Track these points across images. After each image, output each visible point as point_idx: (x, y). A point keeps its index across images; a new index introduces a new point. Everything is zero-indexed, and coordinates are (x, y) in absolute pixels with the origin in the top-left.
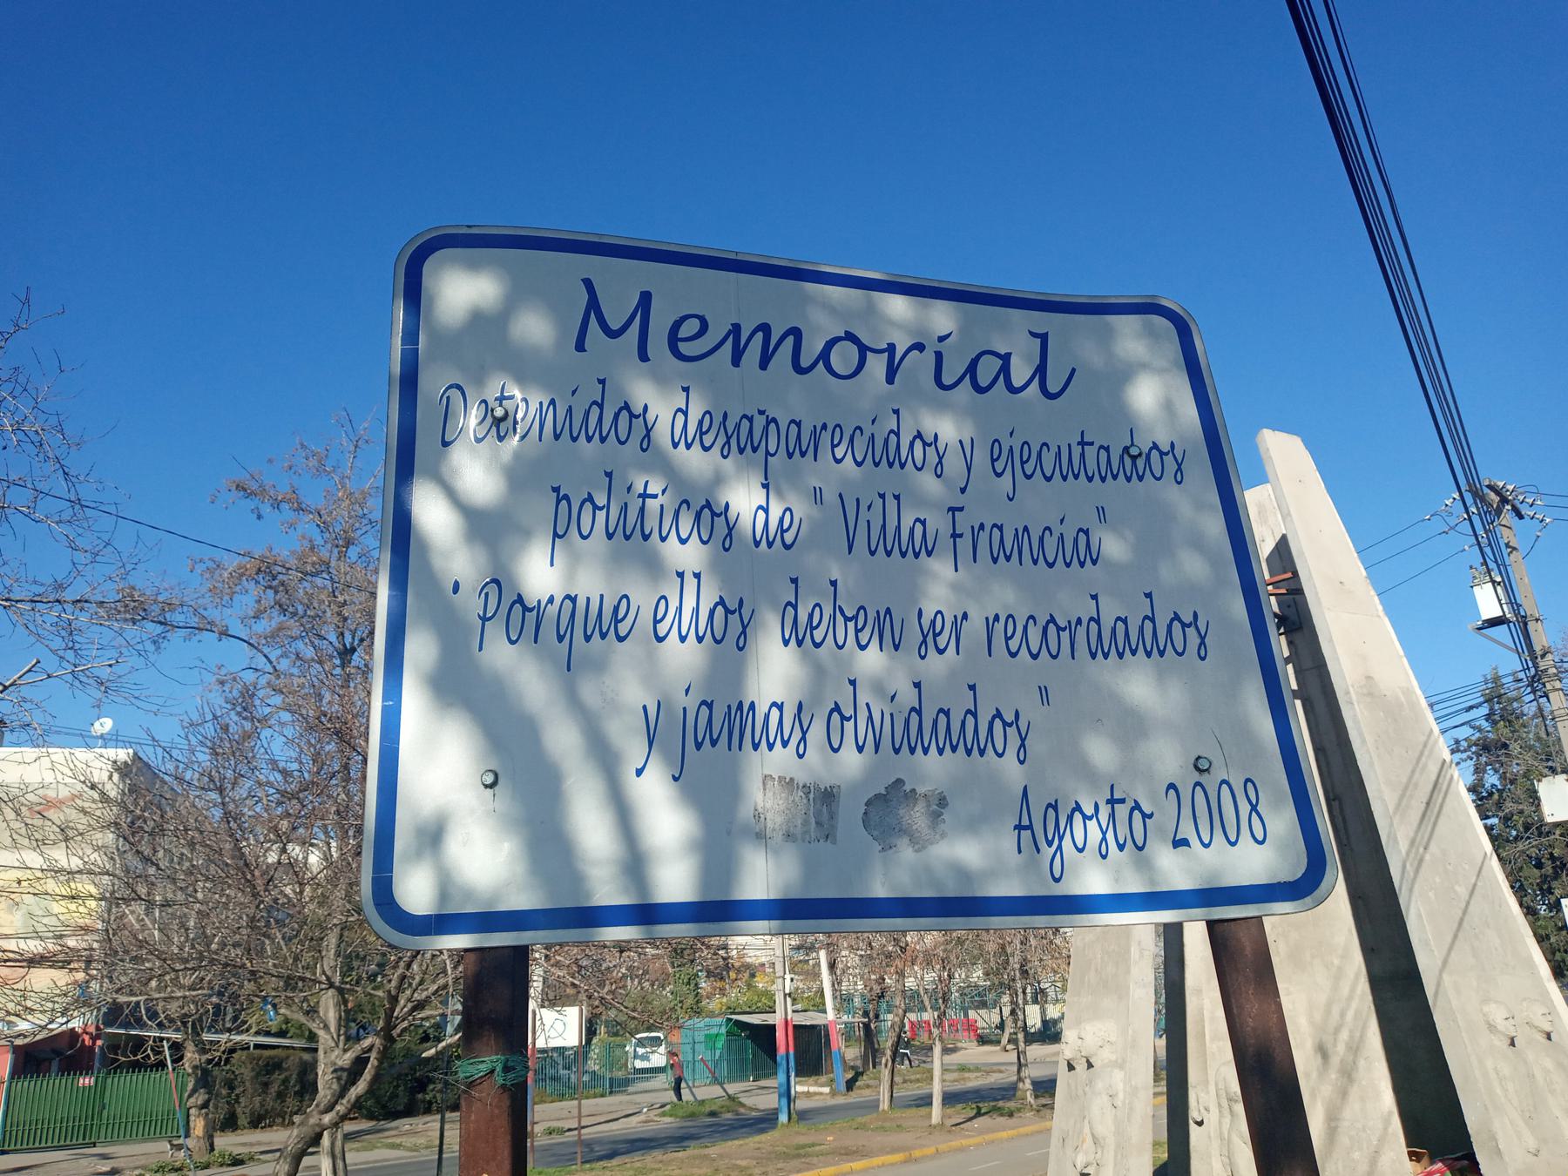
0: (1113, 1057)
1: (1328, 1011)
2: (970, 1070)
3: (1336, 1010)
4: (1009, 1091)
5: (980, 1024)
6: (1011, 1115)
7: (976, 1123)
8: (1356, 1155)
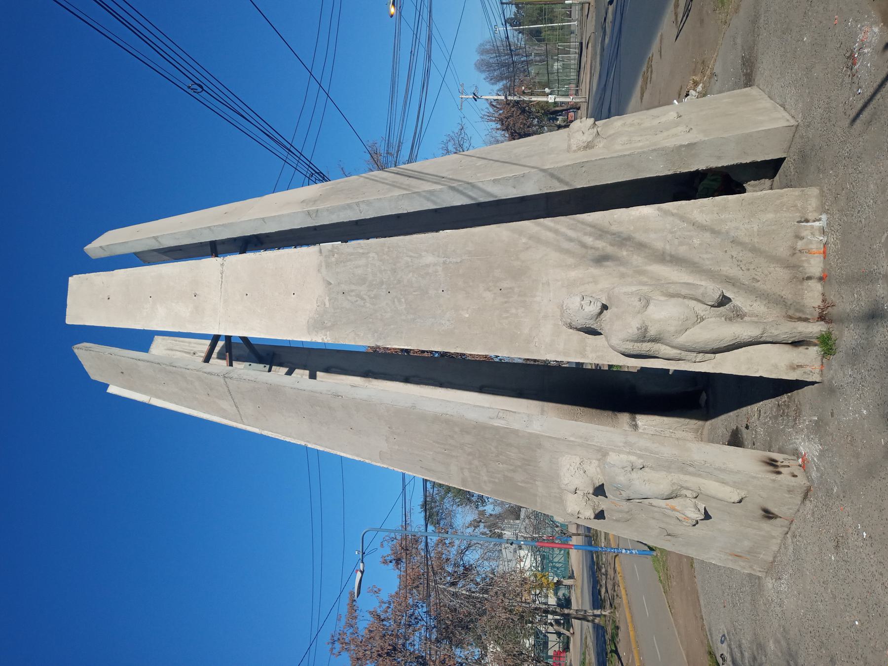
0: (595, 463)
1: (567, 252)
2: (584, 659)
3: (566, 245)
4: (599, 631)
5: (556, 648)
6: (617, 628)
7: (623, 654)
8: (697, 242)
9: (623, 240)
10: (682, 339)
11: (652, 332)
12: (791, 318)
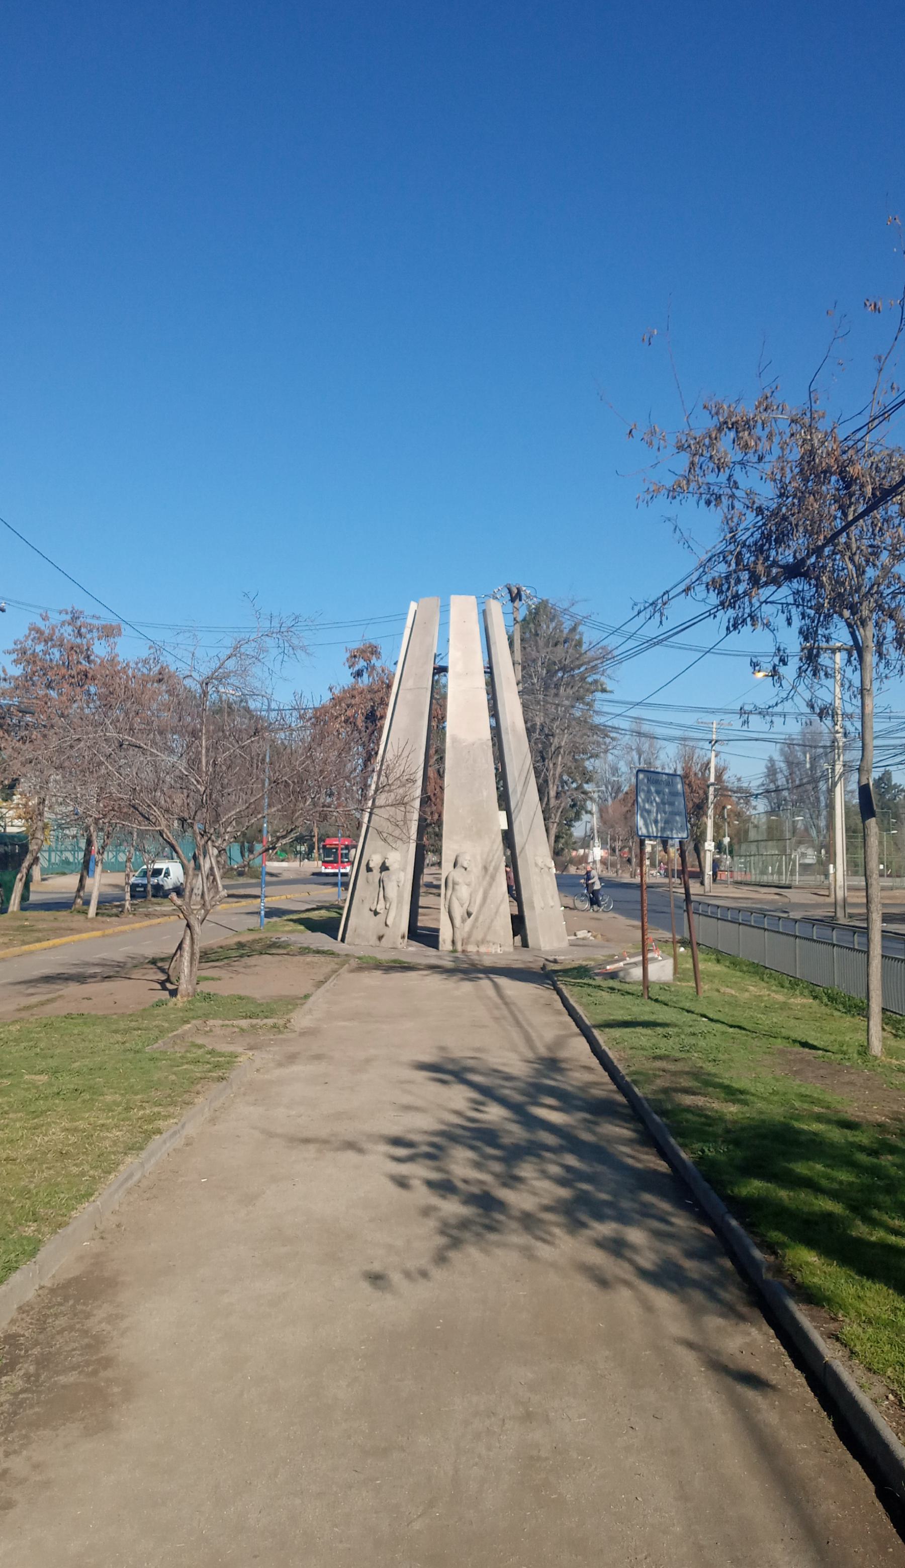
1: (488, 855)
3: (491, 855)
9: (493, 878)
10: (454, 899)
11: (457, 887)
12: (463, 940)
